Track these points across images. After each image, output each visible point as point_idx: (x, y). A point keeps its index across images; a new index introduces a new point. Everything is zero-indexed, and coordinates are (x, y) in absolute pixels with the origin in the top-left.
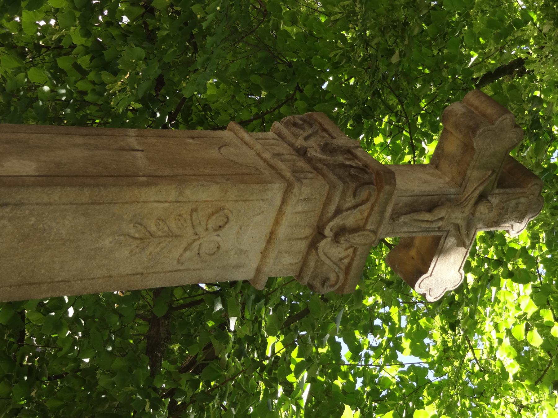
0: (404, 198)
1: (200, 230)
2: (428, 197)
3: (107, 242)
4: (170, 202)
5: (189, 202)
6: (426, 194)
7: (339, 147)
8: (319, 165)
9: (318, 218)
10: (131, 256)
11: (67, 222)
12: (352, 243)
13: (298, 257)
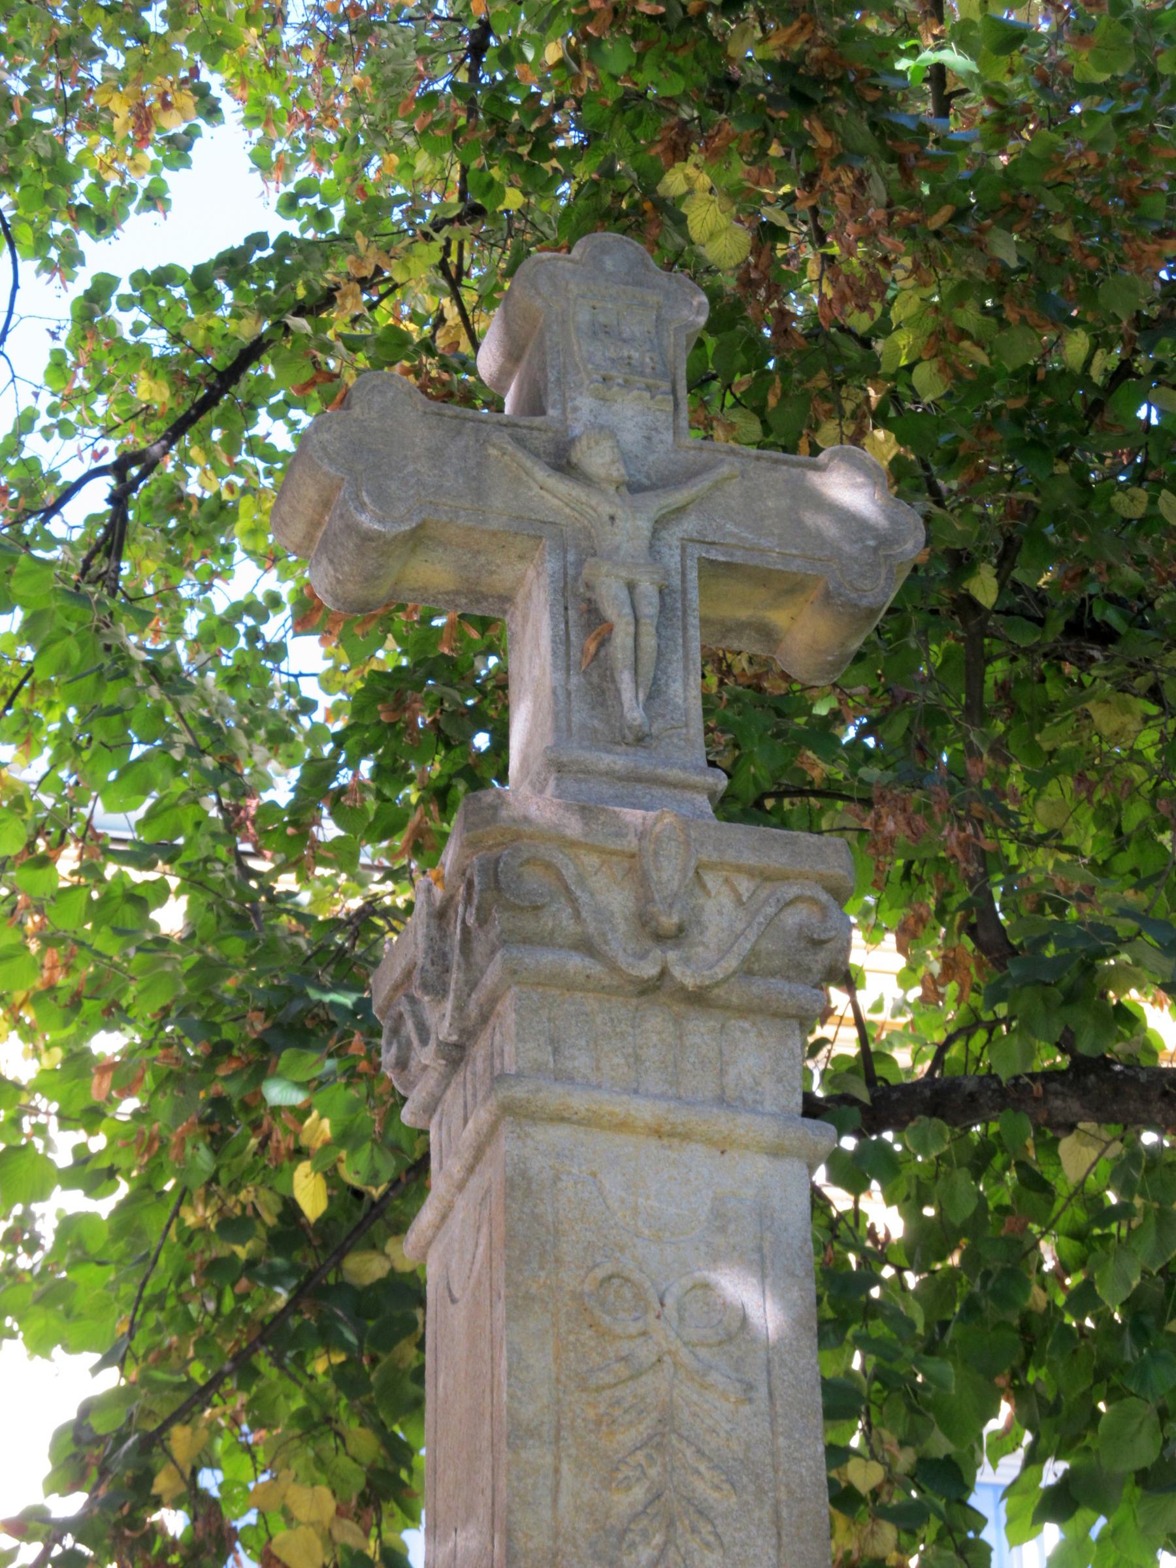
0: (576, 719)
2: (573, 638)
4: (558, 1458)
5: (558, 1401)
6: (562, 648)
7: (431, 947)
8: (473, 1010)
9: (613, 999)
10: (722, 1545)
12: (680, 887)
13: (738, 1034)
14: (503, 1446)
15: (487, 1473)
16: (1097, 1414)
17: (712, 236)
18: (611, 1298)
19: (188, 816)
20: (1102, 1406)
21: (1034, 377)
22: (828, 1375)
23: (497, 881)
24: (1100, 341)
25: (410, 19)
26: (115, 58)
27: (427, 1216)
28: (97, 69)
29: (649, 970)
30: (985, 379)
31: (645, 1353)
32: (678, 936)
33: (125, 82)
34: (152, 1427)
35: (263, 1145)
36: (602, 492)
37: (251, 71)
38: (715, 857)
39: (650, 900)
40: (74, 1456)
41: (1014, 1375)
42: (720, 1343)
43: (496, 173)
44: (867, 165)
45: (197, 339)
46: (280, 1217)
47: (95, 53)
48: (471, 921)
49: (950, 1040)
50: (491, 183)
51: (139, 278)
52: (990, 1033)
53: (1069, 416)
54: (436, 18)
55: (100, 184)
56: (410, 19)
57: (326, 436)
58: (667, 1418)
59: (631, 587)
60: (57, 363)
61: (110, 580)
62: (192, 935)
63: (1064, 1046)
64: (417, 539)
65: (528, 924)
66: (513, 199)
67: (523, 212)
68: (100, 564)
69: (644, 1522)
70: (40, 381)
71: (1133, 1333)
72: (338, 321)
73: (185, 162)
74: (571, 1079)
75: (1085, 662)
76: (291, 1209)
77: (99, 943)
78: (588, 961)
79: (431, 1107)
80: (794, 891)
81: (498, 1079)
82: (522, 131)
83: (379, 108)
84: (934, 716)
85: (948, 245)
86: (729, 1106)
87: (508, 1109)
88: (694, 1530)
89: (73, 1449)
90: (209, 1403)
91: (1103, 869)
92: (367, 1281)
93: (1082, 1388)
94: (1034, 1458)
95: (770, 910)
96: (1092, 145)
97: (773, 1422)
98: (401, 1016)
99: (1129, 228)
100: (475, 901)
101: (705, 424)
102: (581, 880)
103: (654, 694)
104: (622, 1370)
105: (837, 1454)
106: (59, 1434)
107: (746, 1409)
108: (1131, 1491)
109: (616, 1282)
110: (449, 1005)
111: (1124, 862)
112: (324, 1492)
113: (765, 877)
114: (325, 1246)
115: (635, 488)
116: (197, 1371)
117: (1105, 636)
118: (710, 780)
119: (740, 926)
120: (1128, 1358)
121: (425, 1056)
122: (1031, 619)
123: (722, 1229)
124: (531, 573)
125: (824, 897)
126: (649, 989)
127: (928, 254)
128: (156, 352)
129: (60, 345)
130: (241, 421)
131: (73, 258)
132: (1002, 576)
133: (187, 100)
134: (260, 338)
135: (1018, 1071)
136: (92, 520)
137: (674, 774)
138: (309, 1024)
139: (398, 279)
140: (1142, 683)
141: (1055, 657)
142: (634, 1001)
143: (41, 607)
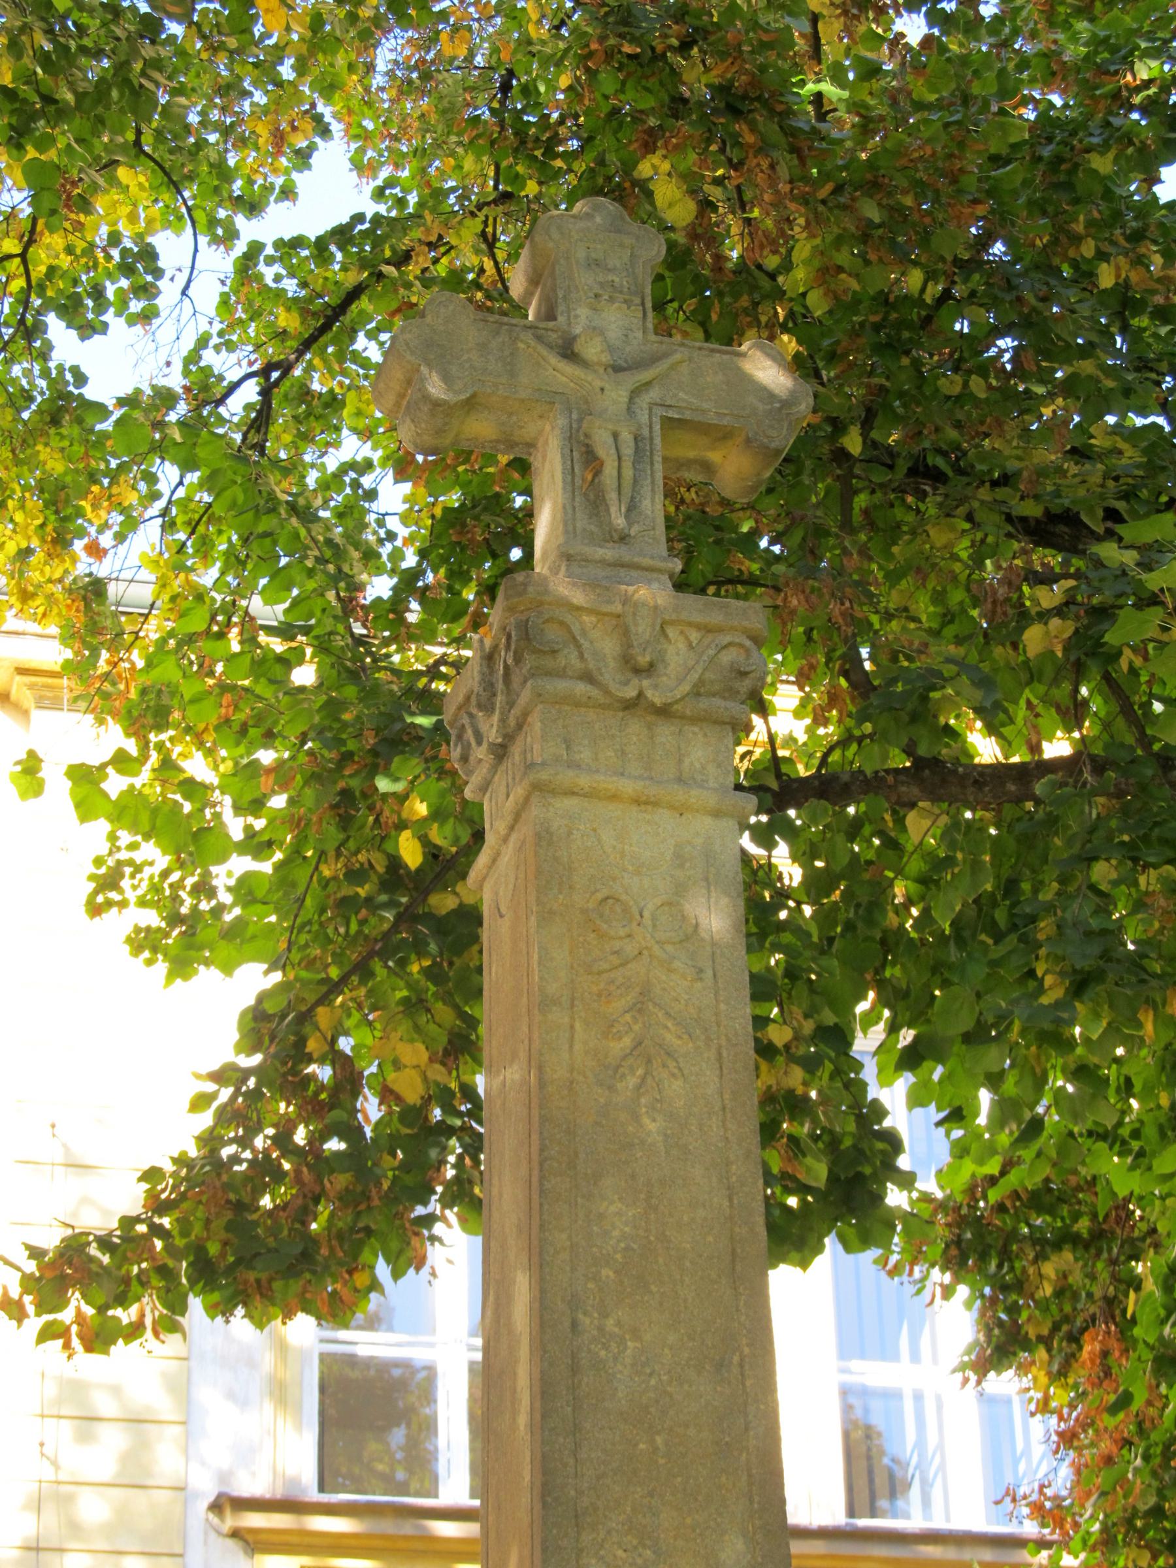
0: (579, 525)
1: (630, 949)
3: (652, 1127)
4: (572, 1018)
5: (572, 981)
8: (512, 722)
11: (612, 1209)
14: (536, 1012)
15: (526, 1029)
16: (934, 997)
17: (670, 205)
18: (607, 912)
19: (317, 605)
20: (937, 993)
21: (886, 301)
22: (754, 970)
23: (527, 634)
24: (931, 276)
25: (459, 68)
26: (260, 98)
27: (483, 859)
28: (246, 105)
29: (630, 693)
30: (855, 304)
31: (630, 949)
32: (650, 669)
33: (266, 113)
34: (304, 1008)
35: (377, 820)
36: (595, 371)
37: (354, 104)
38: (674, 617)
39: (630, 646)
40: (253, 1029)
41: (877, 972)
42: (681, 942)
43: (520, 169)
44: (775, 154)
45: (318, 285)
46: (387, 867)
47: (247, 94)
48: (510, 661)
49: (831, 749)
50: (517, 175)
51: (279, 244)
52: (859, 745)
53: (910, 326)
54: (476, 68)
55: (251, 182)
56: (459, 68)
57: (408, 336)
58: (645, 992)
59: (615, 436)
60: (224, 301)
61: (261, 448)
62: (321, 685)
63: (909, 751)
64: (470, 404)
65: (548, 662)
66: (532, 188)
67: (538, 198)
68: (254, 438)
69: (630, 1061)
70: (213, 313)
71: (956, 943)
72: (412, 270)
73: (308, 167)
74: (579, 766)
75: (922, 496)
76: (395, 863)
77: (258, 690)
78: (589, 687)
79: (484, 788)
80: (727, 639)
81: (530, 766)
82: (537, 140)
83: (440, 128)
84: (820, 532)
85: (830, 209)
86: (686, 783)
87: (537, 787)
88: (664, 1066)
89: (253, 1025)
90: (341, 992)
91: (936, 633)
92: (444, 912)
93: (924, 980)
94: (893, 1029)
95: (711, 652)
96: (929, 141)
97: (716, 994)
98: (463, 726)
99: (952, 197)
100: (513, 647)
101: (664, 330)
102: (584, 633)
103: (632, 508)
104: (615, 960)
105: (761, 1022)
106: (243, 1014)
107: (699, 985)
108: (958, 1048)
109: (610, 901)
110: (496, 718)
111: (950, 631)
112: (421, 1047)
113: (707, 629)
114: (416, 888)
115: (617, 369)
116: (334, 973)
117: (937, 477)
118: (670, 565)
119: (691, 663)
120: (953, 959)
121: (480, 752)
122: (884, 464)
123: (681, 866)
124: (548, 427)
125: (748, 643)
126: (630, 705)
127: (817, 215)
128: (290, 295)
129: (226, 289)
130: (347, 340)
131: (232, 235)
132: (865, 435)
133: (307, 125)
134: (360, 284)
135: (878, 767)
136: (248, 407)
137: (647, 562)
138: (405, 738)
139: (453, 243)
140: (962, 511)
141: (901, 490)
142: (621, 714)
143: (218, 466)
